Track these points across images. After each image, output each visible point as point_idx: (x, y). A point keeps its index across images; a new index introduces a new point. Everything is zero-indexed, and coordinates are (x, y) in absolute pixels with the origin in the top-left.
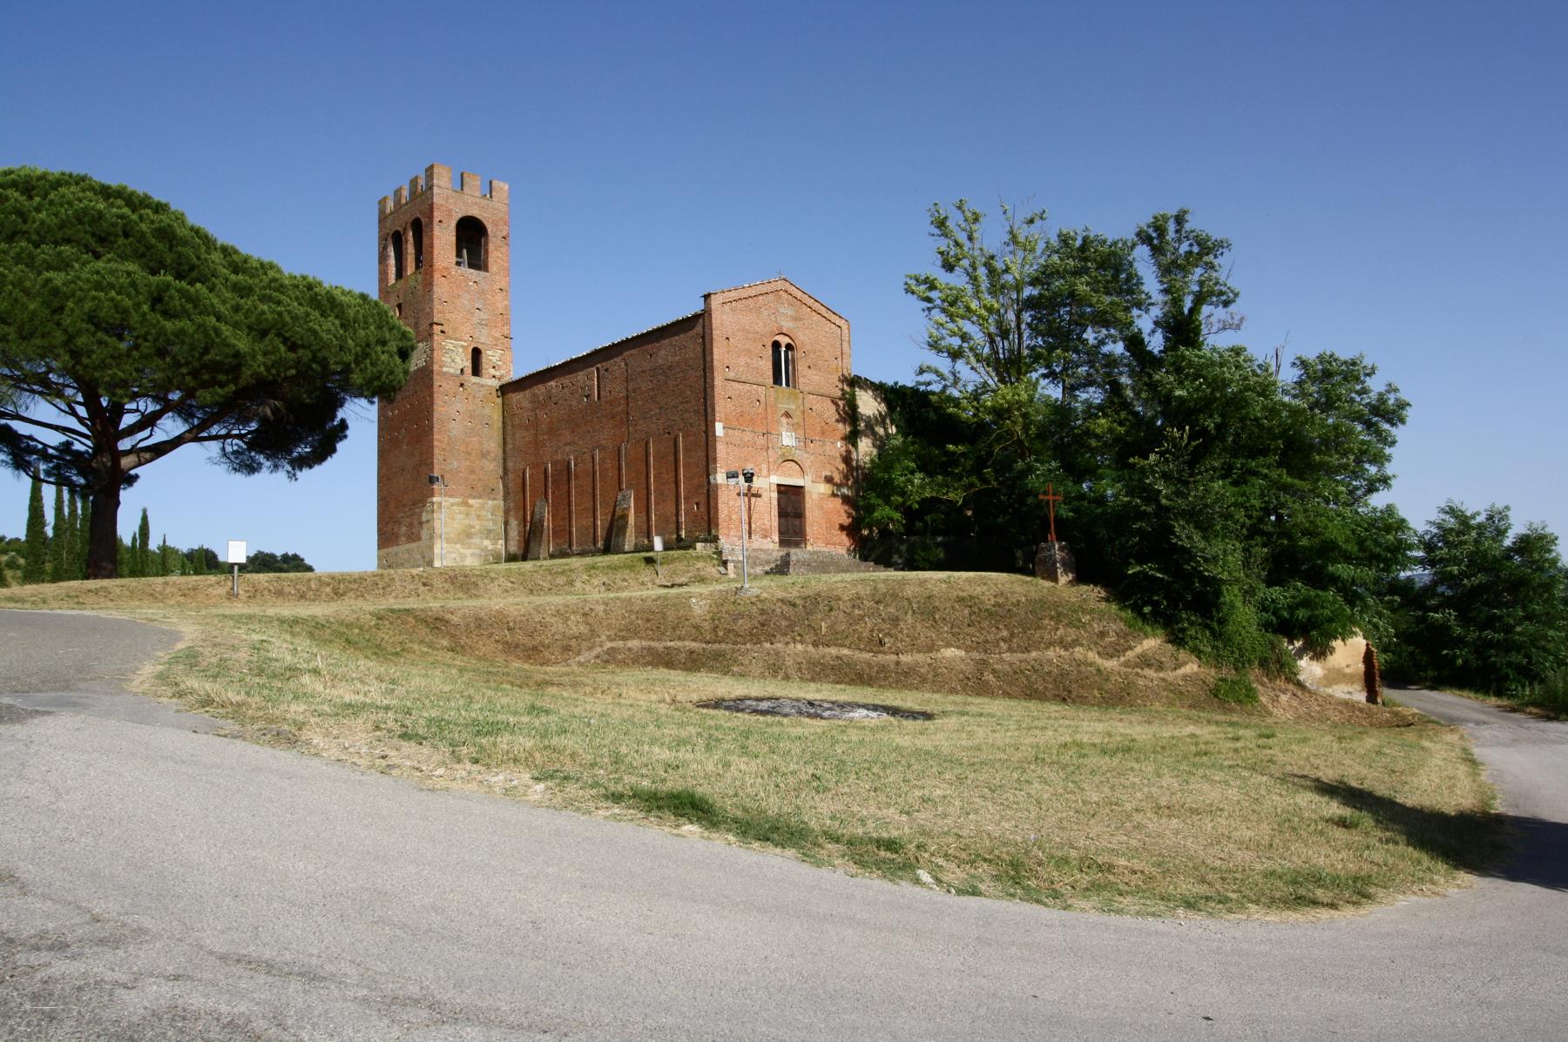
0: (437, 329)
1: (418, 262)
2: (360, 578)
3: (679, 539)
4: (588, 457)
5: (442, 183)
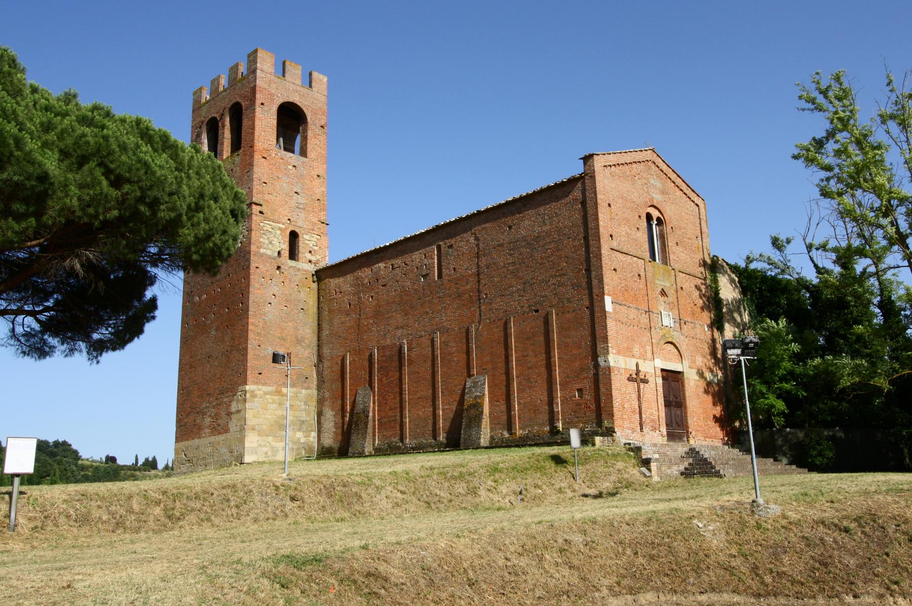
0: (255, 208)
1: (236, 145)
2: (204, 492)
4: (426, 341)
5: (265, 68)
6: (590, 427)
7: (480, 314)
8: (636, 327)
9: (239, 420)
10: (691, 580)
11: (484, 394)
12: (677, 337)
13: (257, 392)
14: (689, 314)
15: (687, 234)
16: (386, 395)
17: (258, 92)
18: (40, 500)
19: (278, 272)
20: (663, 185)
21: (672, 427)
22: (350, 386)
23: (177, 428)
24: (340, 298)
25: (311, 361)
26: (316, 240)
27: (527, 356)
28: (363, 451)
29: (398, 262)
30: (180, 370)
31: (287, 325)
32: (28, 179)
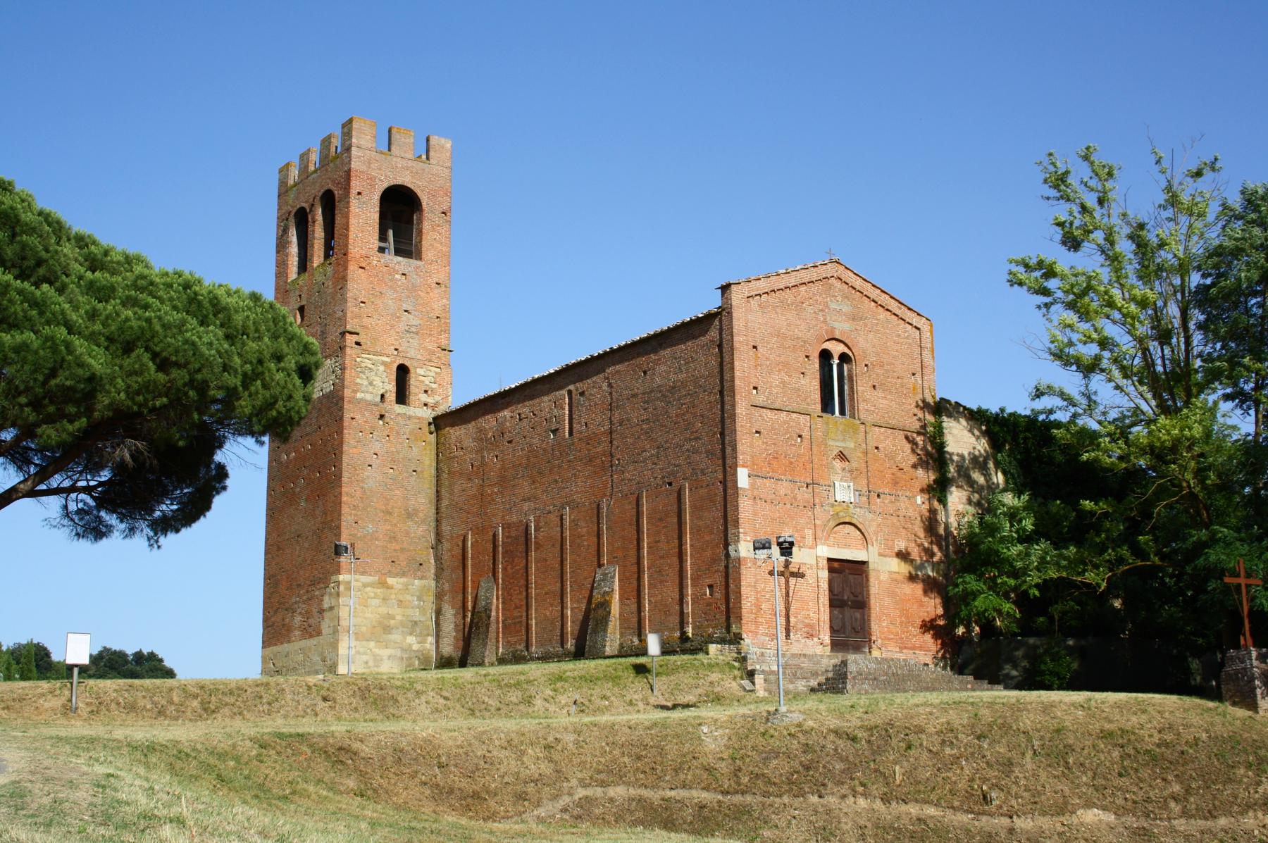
0: (350, 339)
2: (239, 688)
3: (684, 638)
4: (554, 518)
5: (363, 142)
8: (788, 506)
9: (332, 620)
10: (667, 778)
12: (859, 516)
14: (888, 483)
15: (894, 372)
17: (353, 179)
18: (95, 689)
19: (381, 422)
20: (855, 307)
21: (844, 633)
23: (264, 629)
25: (427, 541)
26: (434, 374)
27: (659, 542)
30: (267, 552)
31: (393, 493)
32: (79, 382)
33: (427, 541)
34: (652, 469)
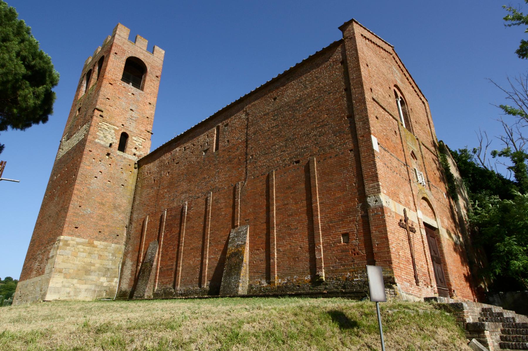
3: (316, 281)
4: (202, 201)
5: (122, 34)
6: (360, 277)
7: (246, 173)
8: (398, 175)
9: (51, 264)
11: (245, 243)
13: (71, 242)
16: (168, 247)
19: (107, 157)
22: (145, 241)
24: (150, 177)
25: (124, 223)
26: (141, 142)
27: (287, 204)
28: (144, 295)
29: (189, 144)
33: (124, 223)
34: (280, 155)
